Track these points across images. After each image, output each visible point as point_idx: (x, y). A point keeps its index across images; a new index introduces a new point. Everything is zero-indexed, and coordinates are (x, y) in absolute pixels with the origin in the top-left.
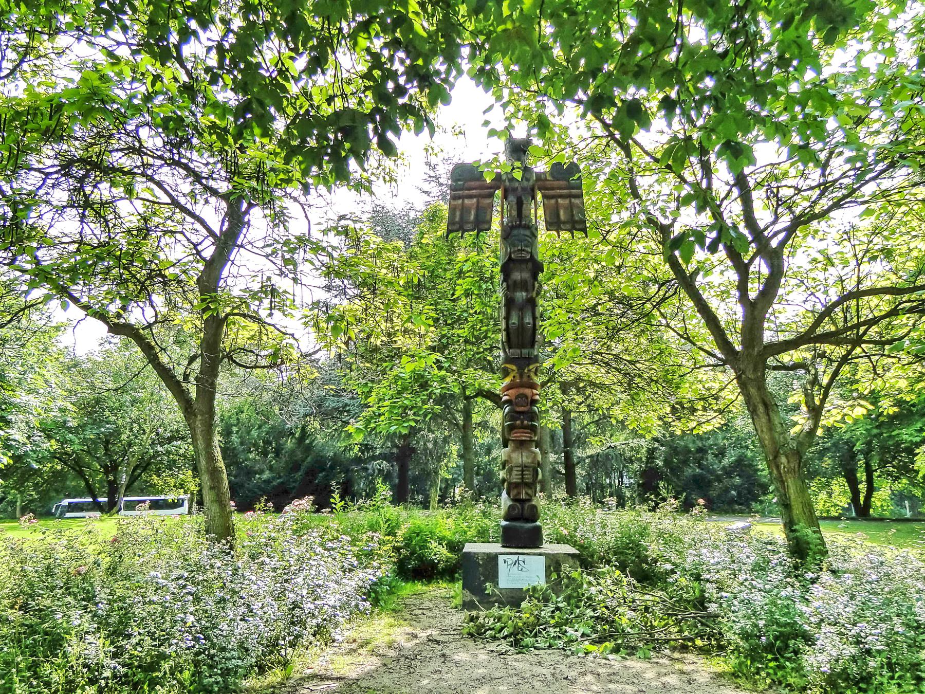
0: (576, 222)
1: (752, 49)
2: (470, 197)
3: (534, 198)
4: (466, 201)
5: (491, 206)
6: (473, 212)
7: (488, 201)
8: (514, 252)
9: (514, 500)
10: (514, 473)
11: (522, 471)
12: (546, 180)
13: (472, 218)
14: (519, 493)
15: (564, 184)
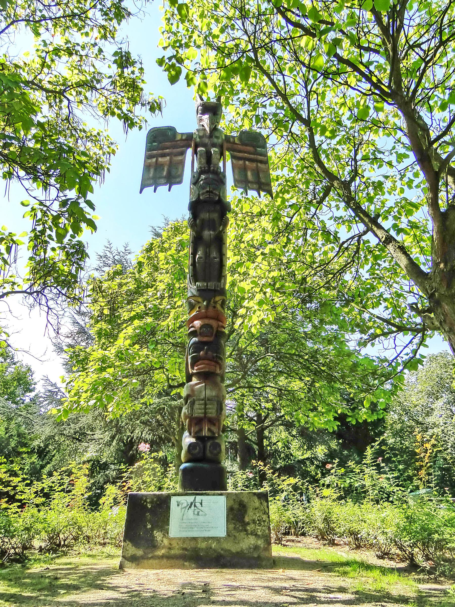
0: (263, 184)
1: (259, 536)
2: (163, 155)
3: (222, 154)
4: (160, 159)
5: (182, 163)
6: (166, 169)
7: (180, 158)
8: (203, 194)
9: (197, 438)
10: (196, 406)
11: (205, 404)
12: (234, 143)
13: (165, 173)
14: (201, 430)
15: (250, 149)
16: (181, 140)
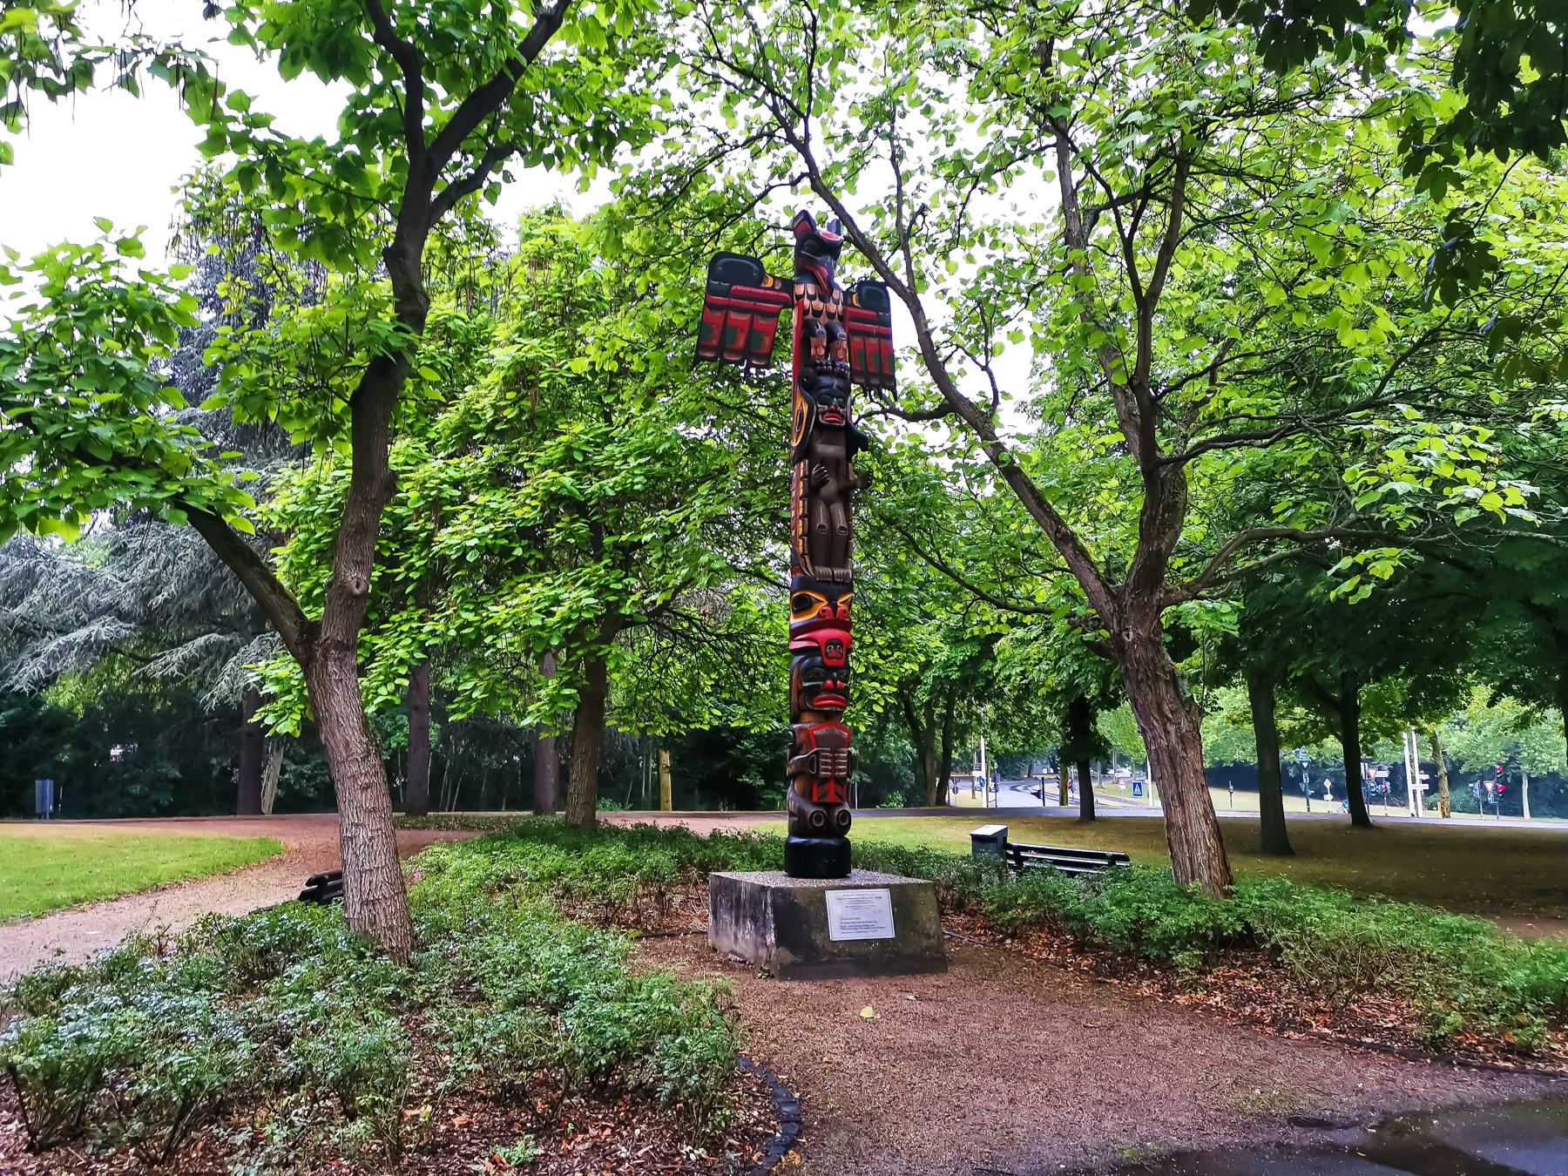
16: (772, 288)
